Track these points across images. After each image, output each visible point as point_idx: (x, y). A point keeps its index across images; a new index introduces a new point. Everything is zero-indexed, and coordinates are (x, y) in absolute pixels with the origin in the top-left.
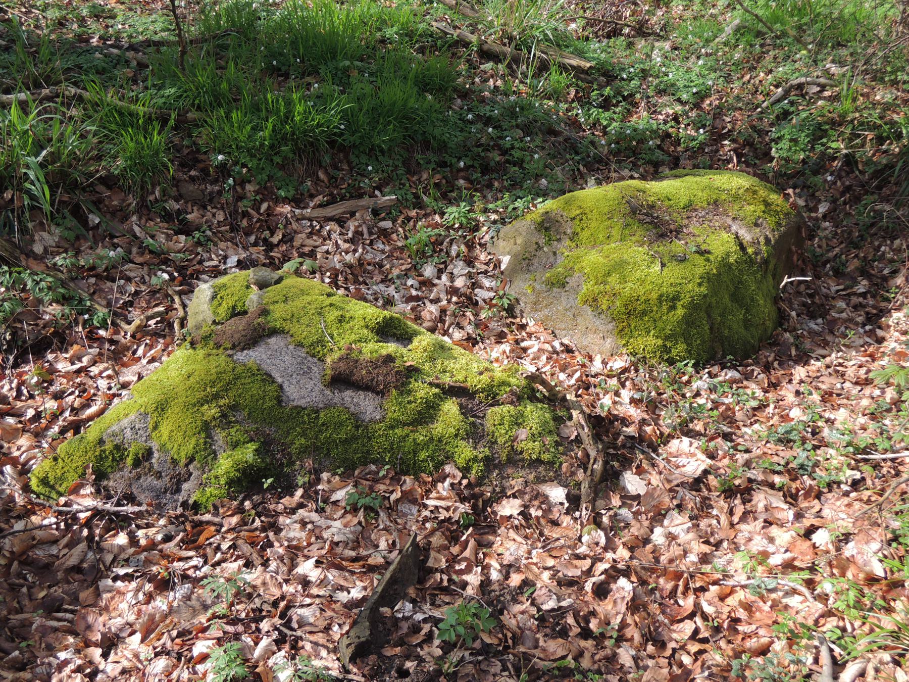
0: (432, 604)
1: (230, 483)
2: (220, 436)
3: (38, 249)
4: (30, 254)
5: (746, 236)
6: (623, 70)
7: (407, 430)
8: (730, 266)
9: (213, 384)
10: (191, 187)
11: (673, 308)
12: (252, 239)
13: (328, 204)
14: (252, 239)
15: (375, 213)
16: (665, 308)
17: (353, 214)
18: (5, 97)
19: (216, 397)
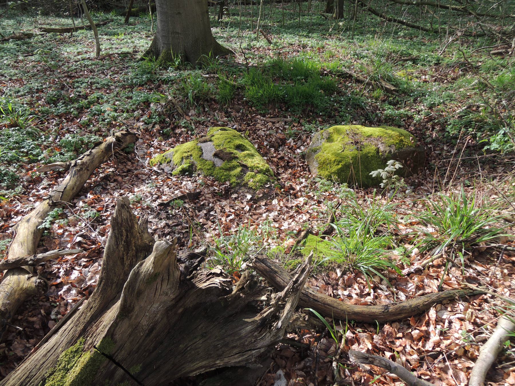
0: (469, 331)
1: (180, 171)
2: (184, 160)
3: (190, 114)
4: (188, 115)
5: (382, 149)
6: (412, 92)
7: (224, 171)
8: (368, 157)
9: (189, 149)
10: (237, 106)
11: (338, 164)
12: (245, 123)
13: (272, 117)
14: (245, 123)
15: (286, 123)
16: (335, 164)
17: (278, 122)
18: (2, 46)
19: (188, 152)
